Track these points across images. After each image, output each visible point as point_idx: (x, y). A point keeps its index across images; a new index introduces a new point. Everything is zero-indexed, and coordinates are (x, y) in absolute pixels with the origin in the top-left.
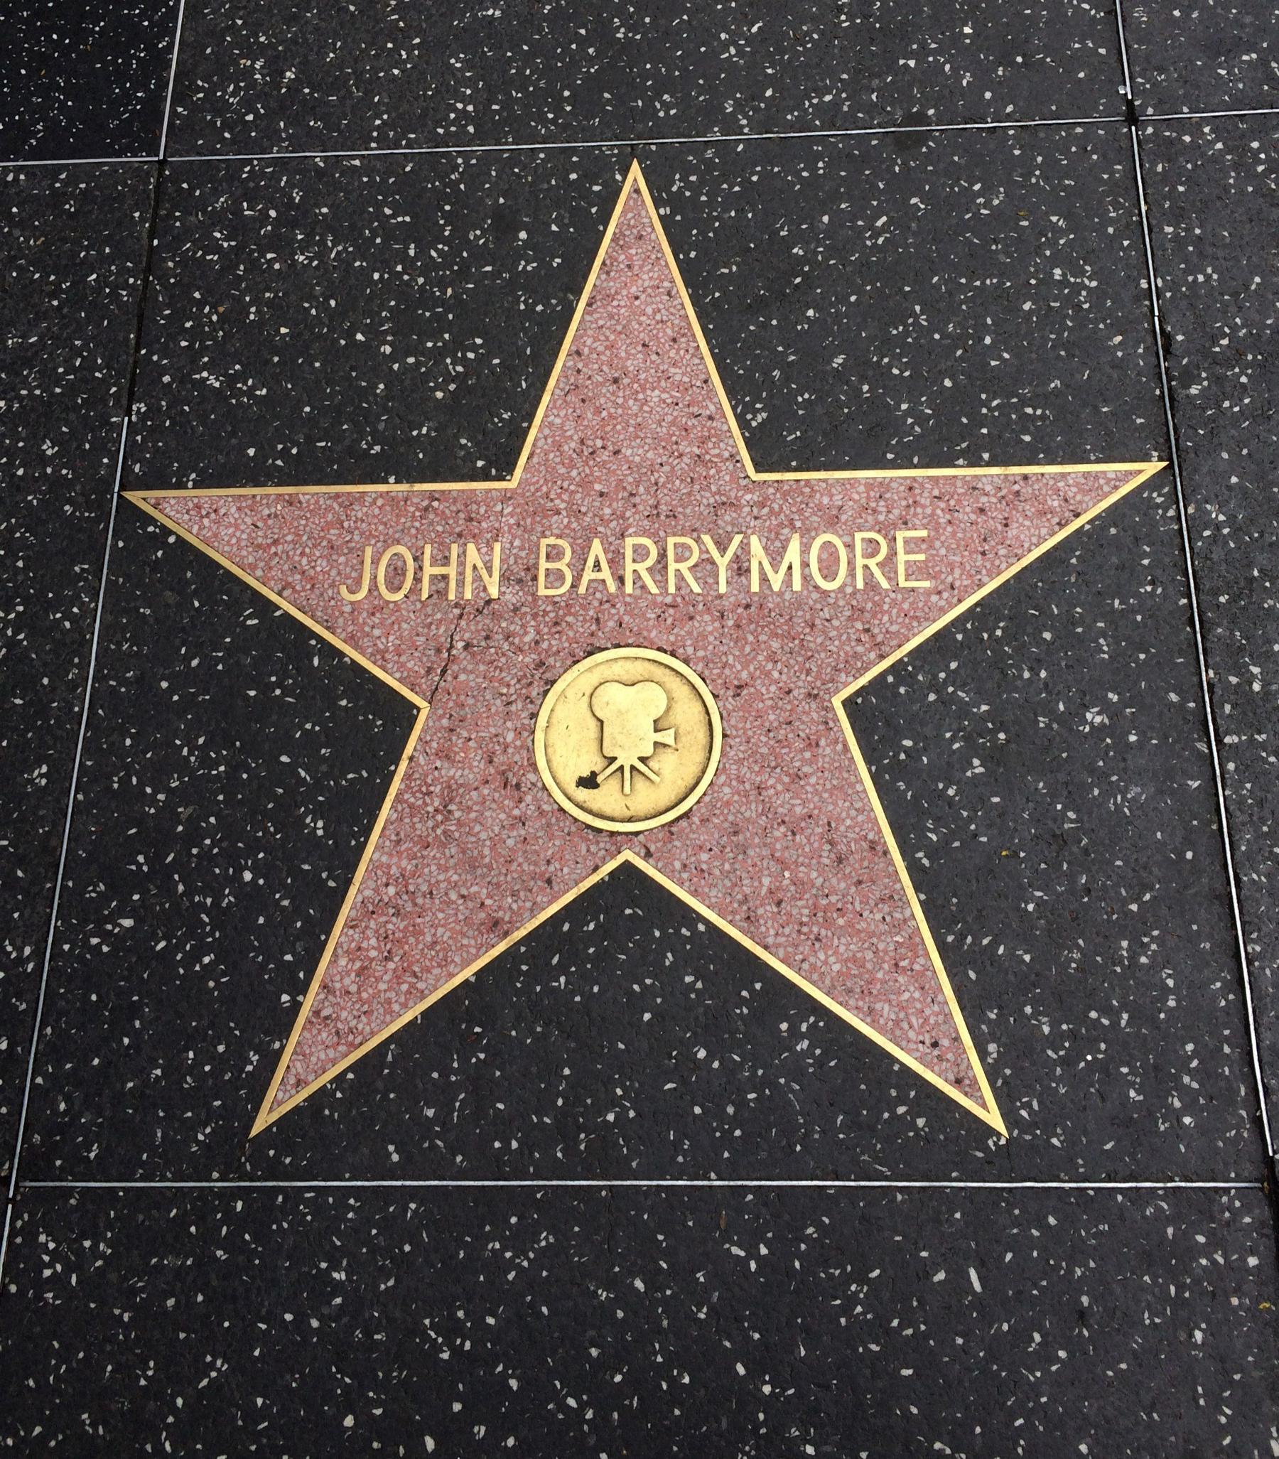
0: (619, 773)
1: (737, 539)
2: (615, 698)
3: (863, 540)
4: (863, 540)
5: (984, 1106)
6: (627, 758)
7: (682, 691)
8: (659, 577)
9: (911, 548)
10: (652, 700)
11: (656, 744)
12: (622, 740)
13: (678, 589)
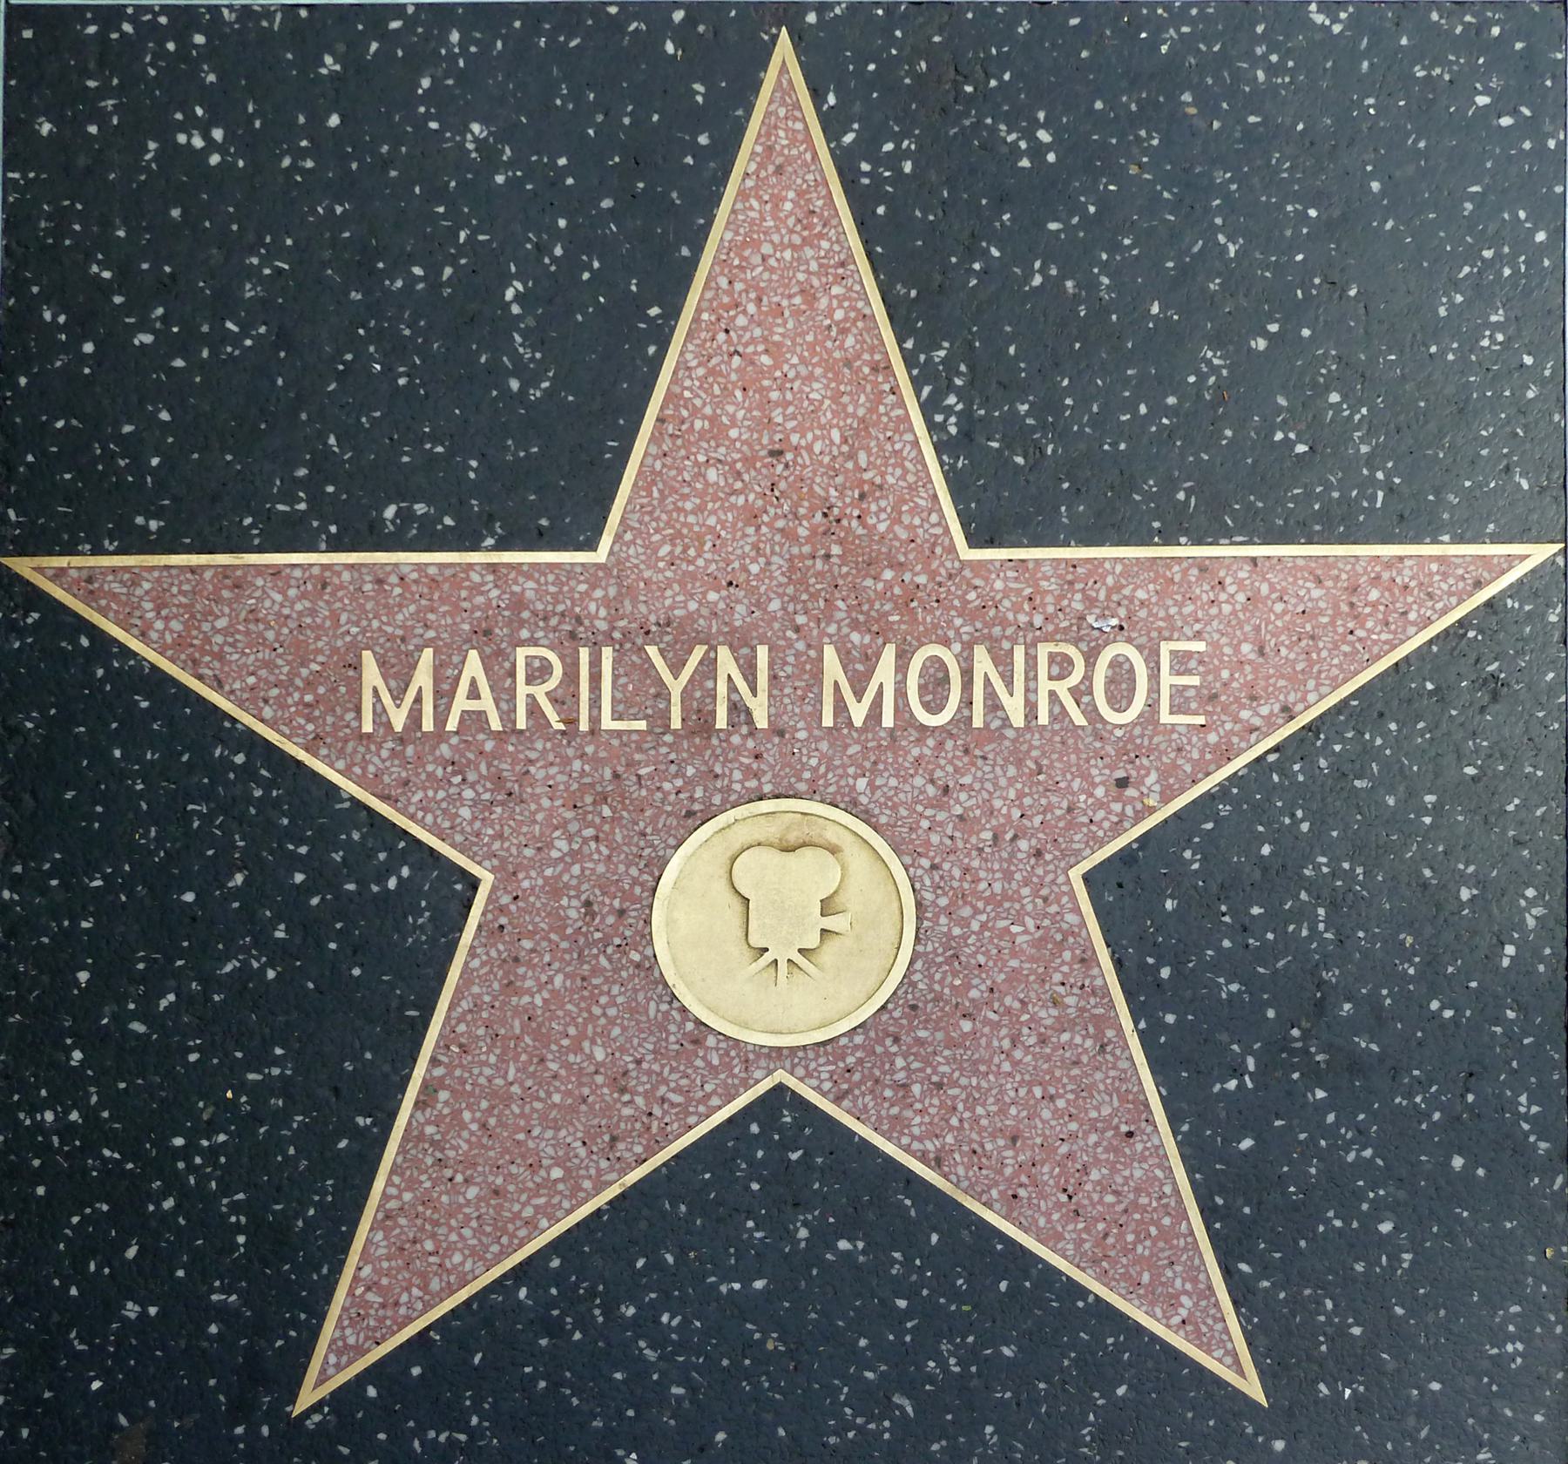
0: (772, 970)
1: (699, 652)
3: (1171, 652)
4: (1171, 652)
7: (858, 860)
8: (504, 706)
12: (776, 943)
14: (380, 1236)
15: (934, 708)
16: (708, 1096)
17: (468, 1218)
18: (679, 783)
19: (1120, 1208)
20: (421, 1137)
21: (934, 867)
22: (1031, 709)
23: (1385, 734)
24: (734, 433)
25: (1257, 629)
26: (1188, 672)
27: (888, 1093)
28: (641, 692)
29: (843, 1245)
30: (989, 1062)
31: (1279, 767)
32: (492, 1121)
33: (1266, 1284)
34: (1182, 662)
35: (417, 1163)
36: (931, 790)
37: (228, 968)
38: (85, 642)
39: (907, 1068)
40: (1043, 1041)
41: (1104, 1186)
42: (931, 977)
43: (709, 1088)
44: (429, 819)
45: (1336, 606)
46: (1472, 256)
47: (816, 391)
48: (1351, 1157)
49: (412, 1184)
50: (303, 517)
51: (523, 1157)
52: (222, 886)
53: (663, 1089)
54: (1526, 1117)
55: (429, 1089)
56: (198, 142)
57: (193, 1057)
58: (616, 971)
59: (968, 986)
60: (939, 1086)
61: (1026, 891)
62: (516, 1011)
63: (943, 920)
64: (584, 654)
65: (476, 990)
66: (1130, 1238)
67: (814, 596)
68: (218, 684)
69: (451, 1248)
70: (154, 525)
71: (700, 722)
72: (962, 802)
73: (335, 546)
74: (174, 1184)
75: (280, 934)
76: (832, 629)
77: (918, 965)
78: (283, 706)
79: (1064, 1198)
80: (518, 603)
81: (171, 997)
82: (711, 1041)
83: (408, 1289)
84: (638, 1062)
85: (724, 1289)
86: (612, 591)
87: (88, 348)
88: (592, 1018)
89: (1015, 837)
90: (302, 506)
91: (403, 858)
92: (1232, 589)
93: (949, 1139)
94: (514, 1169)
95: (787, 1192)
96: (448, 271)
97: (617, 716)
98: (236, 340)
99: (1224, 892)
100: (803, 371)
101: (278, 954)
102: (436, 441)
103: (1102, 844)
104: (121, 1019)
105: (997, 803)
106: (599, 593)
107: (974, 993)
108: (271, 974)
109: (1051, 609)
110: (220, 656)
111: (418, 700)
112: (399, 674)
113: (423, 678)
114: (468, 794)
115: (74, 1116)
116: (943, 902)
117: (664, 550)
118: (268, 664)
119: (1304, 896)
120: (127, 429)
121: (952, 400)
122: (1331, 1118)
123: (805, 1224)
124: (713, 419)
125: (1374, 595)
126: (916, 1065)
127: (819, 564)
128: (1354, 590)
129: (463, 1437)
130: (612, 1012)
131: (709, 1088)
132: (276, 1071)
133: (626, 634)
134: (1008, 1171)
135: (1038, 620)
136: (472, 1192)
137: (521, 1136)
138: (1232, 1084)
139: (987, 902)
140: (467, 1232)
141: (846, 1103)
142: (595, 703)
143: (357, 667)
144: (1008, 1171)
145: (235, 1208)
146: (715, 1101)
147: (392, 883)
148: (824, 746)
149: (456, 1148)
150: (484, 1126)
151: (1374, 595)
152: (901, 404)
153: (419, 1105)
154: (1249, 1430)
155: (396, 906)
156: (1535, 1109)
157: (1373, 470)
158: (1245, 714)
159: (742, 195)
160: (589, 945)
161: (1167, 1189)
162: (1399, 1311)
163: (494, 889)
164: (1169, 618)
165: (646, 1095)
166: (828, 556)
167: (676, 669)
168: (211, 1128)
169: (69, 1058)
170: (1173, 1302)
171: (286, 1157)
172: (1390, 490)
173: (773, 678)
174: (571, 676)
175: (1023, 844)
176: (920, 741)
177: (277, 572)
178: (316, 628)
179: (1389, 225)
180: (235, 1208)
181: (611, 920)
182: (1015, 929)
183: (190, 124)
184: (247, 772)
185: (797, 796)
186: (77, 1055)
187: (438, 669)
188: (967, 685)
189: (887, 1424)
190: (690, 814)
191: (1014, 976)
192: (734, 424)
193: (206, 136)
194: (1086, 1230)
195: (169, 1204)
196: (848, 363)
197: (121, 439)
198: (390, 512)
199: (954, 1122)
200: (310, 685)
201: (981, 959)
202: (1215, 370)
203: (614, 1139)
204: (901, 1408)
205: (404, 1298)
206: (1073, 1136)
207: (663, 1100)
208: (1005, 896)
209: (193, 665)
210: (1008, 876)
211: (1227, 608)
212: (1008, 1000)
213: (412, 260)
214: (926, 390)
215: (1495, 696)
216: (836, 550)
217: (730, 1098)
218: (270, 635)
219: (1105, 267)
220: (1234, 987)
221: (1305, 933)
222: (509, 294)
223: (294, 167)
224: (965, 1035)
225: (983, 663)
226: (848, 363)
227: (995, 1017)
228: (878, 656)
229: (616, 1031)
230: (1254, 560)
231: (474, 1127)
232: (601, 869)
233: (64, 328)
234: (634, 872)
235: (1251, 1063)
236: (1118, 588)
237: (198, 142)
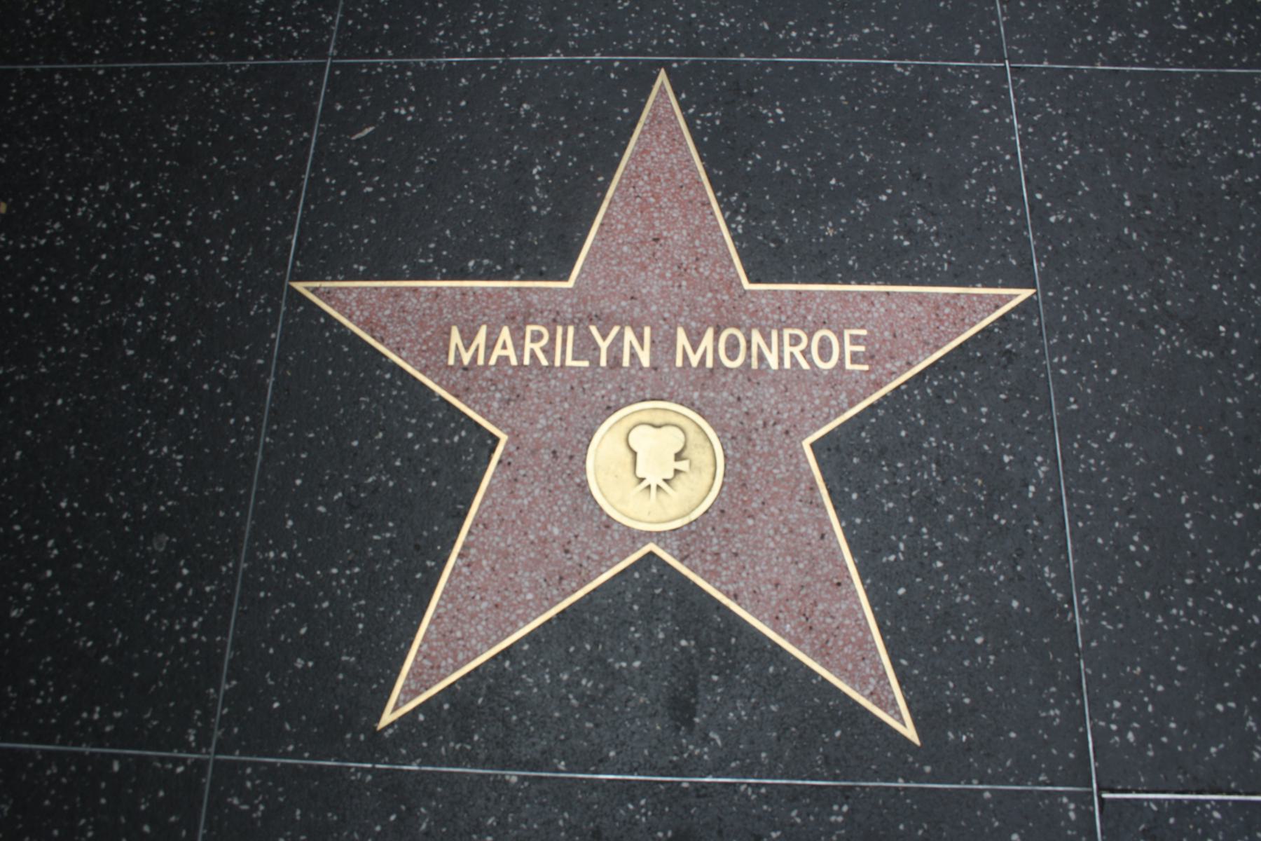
1: (616, 330)
2: (641, 438)
5: (1011, 297)
6: (654, 480)
9: (850, 342)
10: (672, 440)
11: (677, 472)
12: (649, 475)
13: (632, 364)
14: (433, 627)
15: (733, 357)
16: (612, 557)
17: (481, 619)
18: (603, 392)
19: (834, 626)
20: (459, 574)
21: (733, 438)
22: (781, 359)
23: (959, 377)
24: (636, 231)
25: (891, 325)
26: (858, 344)
27: (709, 558)
28: (585, 347)
29: (684, 643)
30: (762, 542)
31: (906, 392)
32: (497, 566)
33: (916, 672)
34: (855, 340)
35: (457, 588)
36: (731, 399)
37: (370, 480)
38: (322, 320)
39: (718, 544)
40: (791, 531)
41: (826, 613)
42: (731, 496)
43: (613, 552)
44: (477, 407)
45: (929, 315)
46: (978, 163)
47: (676, 213)
48: (958, 600)
49: (452, 599)
50: (430, 266)
51: (513, 586)
52: (372, 438)
53: (588, 552)
54: (1049, 579)
55: (465, 546)
56: (403, 112)
57: (347, 526)
58: (567, 487)
59: (751, 500)
60: (736, 555)
61: (781, 452)
62: (514, 507)
63: (738, 465)
64: (560, 330)
65: (494, 495)
66: (841, 643)
67: (673, 305)
68: (382, 341)
69: (471, 636)
70: (362, 268)
71: (615, 361)
72: (747, 405)
73: (444, 278)
74: (330, 596)
75: (398, 463)
76: (682, 319)
77: (725, 489)
78: (411, 351)
79: (803, 619)
80: (530, 305)
81: (340, 494)
82: (615, 527)
83: (445, 659)
84: (576, 536)
85: (617, 666)
86: (575, 300)
87: (343, 193)
88: (553, 513)
89: (775, 424)
90: (431, 261)
91: (462, 427)
92: (878, 306)
93: (742, 584)
94: (507, 593)
95: (650, 614)
96: (508, 162)
97: (575, 359)
98: (409, 190)
99: (882, 452)
100: (669, 204)
101: (394, 472)
102: (495, 232)
103: (819, 428)
104: (313, 506)
105: (765, 406)
106: (568, 301)
107: (754, 505)
108: (391, 484)
109: (789, 313)
110: (384, 328)
111: (477, 350)
112: (468, 339)
113: (481, 338)
114: (498, 395)
115: (284, 555)
116: (738, 455)
117: (601, 282)
118: (406, 332)
119: (924, 458)
120: (355, 227)
121: (739, 218)
122: (946, 578)
123: (663, 630)
124: (626, 225)
125: (947, 310)
126: (724, 543)
127: (676, 290)
128: (938, 308)
129: (469, 747)
130: (564, 509)
131: (613, 552)
132: (388, 535)
133: (581, 320)
134: (774, 603)
135: (783, 318)
136: (484, 605)
137: (512, 575)
138: (892, 558)
139: (760, 456)
140: (480, 628)
141: (686, 562)
142: (564, 352)
143: (449, 333)
144: (774, 603)
145: (360, 608)
146: (616, 559)
147: (456, 439)
148: (677, 376)
149: (477, 580)
150: (493, 569)
151: (947, 310)
152: (715, 219)
153: (460, 556)
154: (911, 759)
155: (455, 453)
156: (1053, 575)
157: (941, 254)
158: (888, 366)
159: (643, 132)
160: (554, 473)
161: (860, 616)
162: (990, 689)
163: (507, 443)
164: (848, 319)
165: (580, 555)
166: (680, 286)
167: (604, 337)
168: (351, 564)
169: (285, 524)
170: (865, 683)
171: (389, 582)
172: (950, 263)
173: (653, 342)
174: (552, 340)
175: (779, 427)
176: (725, 375)
177: (415, 290)
178: (432, 316)
179: (938, 150)
180: (360, 608)
181: (566, 460)
182: (775, 471)
183: (401, 105)
184: (391, 383)
185: (662, 400)
186: (290, 523)
187: (488, 334)
188: (749, 348)
189: (706, 749)
190: (609, 408)
191: (775, 496)
192: (636, 226)
193: (407, 110)
194: (816, 638)
195: (326, 605)
196: (691, 202)
197: (352, 231)
198: (471, 264)
199: (744, 575)
200: (425, 342)
201: (758, 486)
202: (864, 208)
203: (561, 579)
204: (714, 740)
205: (443, 664)
206: (809, 585)
207: (588, 558)
208: (770, 454)
209: (372, 333)
210: (771, 443)
211: (876, 315)
212: (773, 509)
213: (492, 157)
214: (727, 214)
215: (1010, 361)
216: (684, 283)
217: (624, 557)
218: (409, 318)
219: (810, 165)
220: (891, 505)
221: (926, 477)
222: (535, 171)
223: (444, 121)
224: (750, 527)
225: (756, 337)
226: (691, 202)
227: (764, 517)
228: (704, 332)
229: (565, 520)
230: (888, 293)
231: (488, 569)
232: (562, 434)
233: (334, 185)
234: (579, 436)
235: (902, 546)
236: (822, 304)
237: (403, 112)
